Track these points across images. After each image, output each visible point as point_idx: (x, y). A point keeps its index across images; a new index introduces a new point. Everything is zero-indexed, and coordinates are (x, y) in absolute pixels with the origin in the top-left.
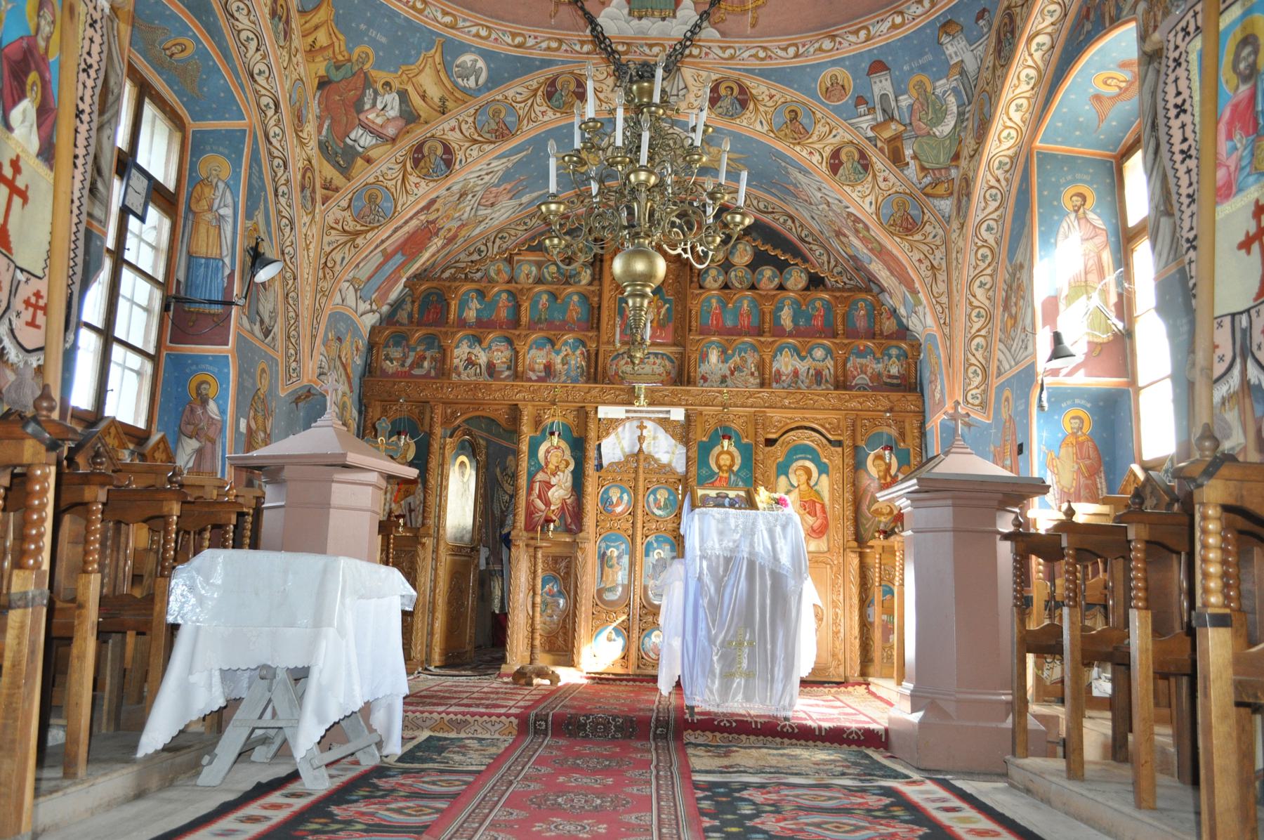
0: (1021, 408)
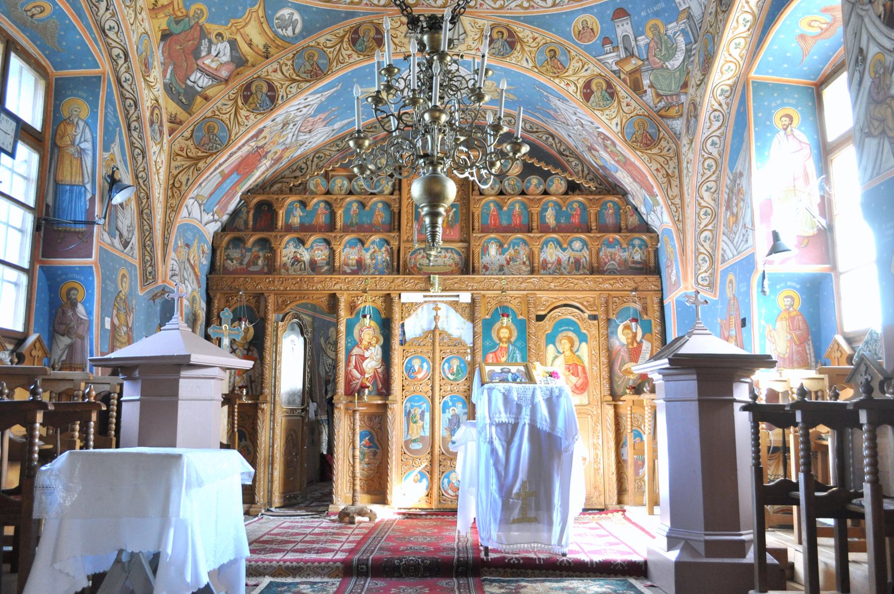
0: (743, 289)
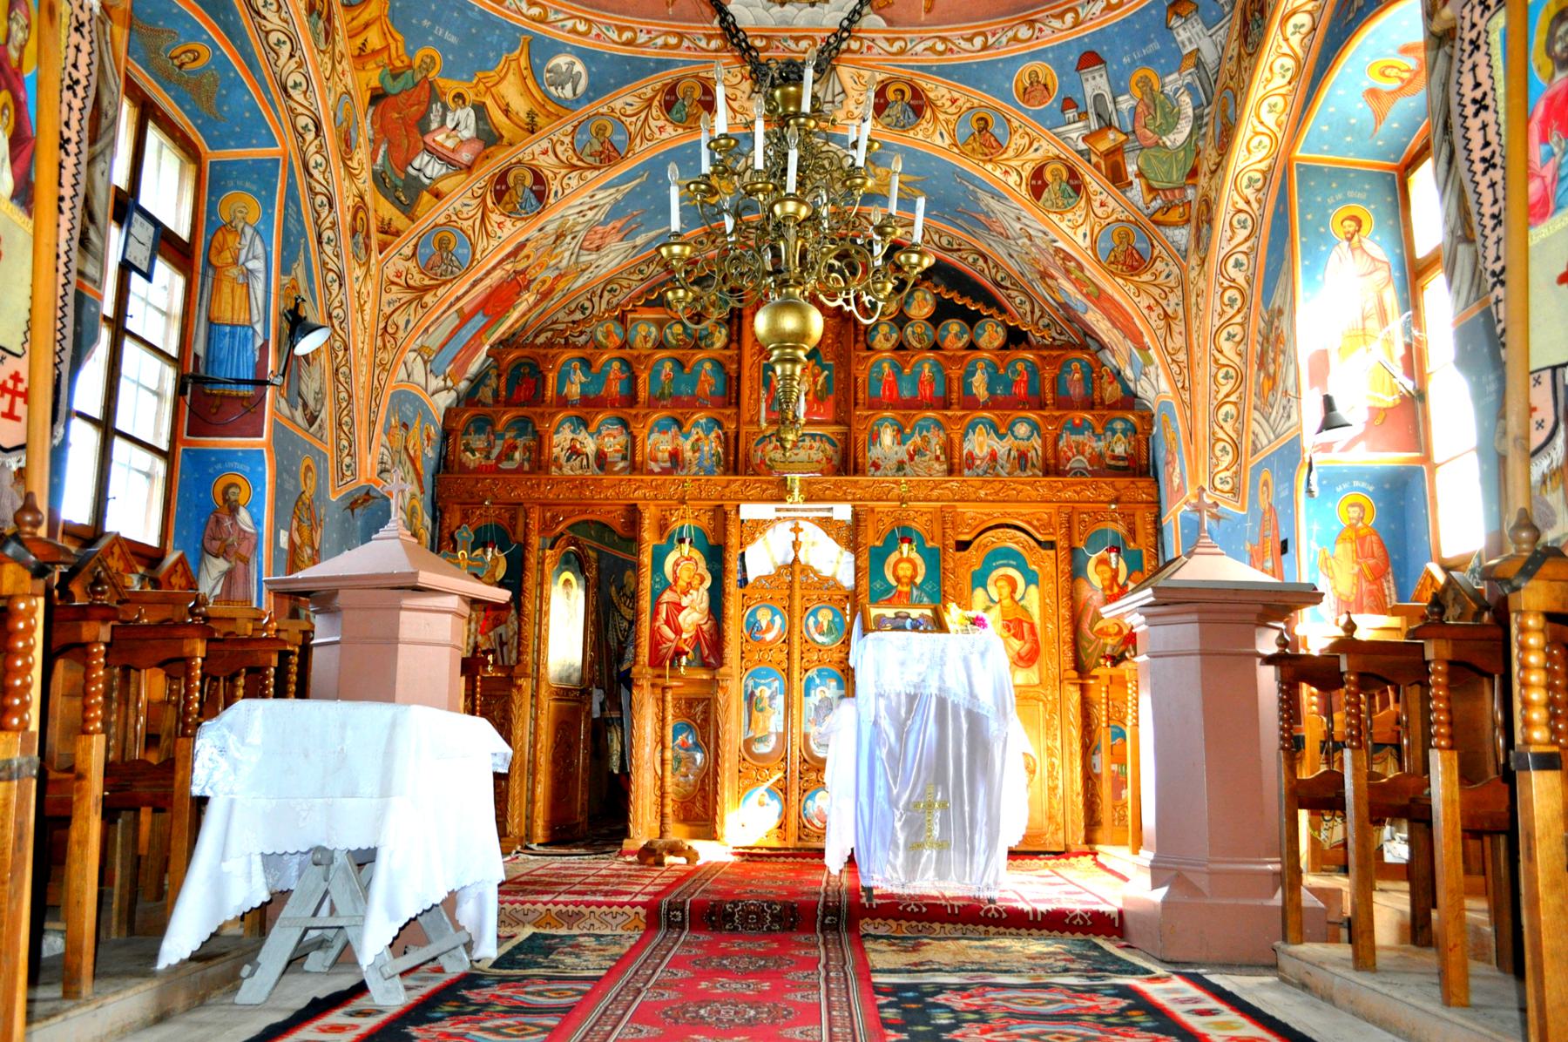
0: (1284, 494)
